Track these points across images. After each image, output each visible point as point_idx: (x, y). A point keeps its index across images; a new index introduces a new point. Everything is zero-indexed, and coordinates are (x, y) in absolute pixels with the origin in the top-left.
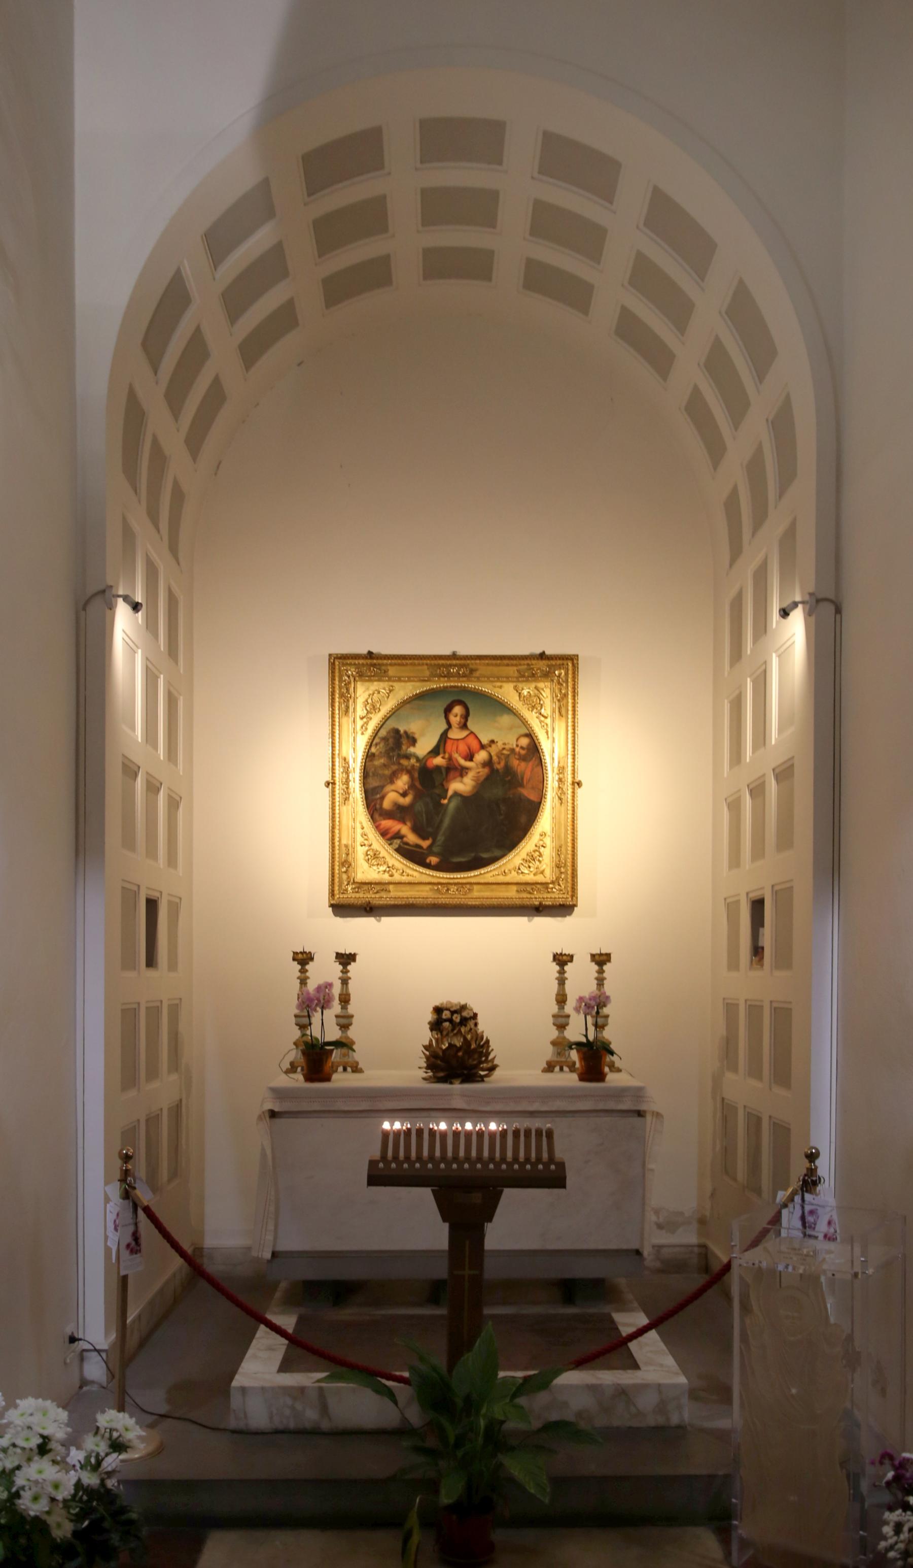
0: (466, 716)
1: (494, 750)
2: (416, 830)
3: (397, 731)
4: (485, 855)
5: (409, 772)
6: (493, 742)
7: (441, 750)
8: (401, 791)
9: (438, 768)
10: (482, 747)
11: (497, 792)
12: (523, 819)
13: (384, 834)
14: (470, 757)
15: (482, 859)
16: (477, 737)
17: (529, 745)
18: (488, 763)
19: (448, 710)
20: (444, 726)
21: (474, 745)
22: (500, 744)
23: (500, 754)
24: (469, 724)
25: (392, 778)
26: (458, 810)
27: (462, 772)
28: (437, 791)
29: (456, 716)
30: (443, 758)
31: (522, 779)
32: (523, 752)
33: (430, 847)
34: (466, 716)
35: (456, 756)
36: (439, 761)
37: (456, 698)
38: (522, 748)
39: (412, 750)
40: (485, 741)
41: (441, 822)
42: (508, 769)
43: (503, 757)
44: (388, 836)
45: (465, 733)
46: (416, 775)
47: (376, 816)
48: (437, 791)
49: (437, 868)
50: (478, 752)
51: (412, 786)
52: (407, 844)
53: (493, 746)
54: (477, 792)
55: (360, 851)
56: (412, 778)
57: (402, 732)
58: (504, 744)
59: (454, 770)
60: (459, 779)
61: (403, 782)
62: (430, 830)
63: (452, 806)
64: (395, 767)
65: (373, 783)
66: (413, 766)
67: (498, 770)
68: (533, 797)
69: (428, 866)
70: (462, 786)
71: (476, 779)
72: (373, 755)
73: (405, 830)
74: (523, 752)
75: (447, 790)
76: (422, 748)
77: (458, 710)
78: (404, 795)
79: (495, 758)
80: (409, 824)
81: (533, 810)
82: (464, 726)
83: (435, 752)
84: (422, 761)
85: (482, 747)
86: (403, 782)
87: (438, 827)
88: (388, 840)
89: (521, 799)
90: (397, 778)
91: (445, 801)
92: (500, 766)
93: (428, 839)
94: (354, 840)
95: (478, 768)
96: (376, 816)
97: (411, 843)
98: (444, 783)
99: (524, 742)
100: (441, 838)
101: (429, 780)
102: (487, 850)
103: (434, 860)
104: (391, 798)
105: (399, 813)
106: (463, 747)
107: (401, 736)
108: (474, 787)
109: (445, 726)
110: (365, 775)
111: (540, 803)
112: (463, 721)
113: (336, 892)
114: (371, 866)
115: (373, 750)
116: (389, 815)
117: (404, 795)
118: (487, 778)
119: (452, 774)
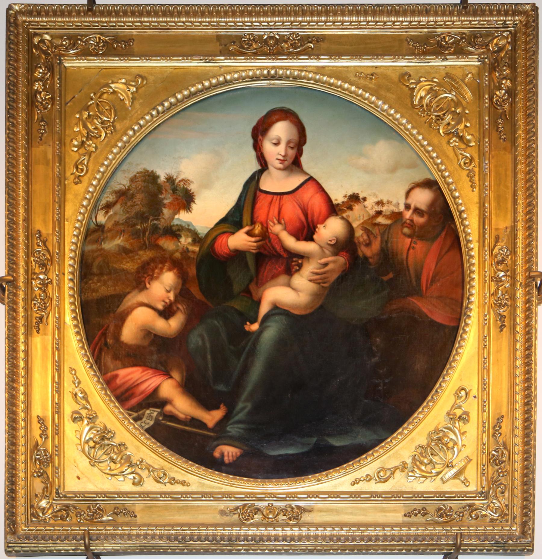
0: (299, 142)
1: (357, 217)
2: (189, 388)
3: (151, 177)
4: (336, 442)
5: (177, 264)
6: (355, 198)
7: (246, 218)
8: (160, 306)
9: (239, 255)
10: (333, 209)
11: (363, 307)
12: (420, 364)
13: (123, 396)
14: (306, 232)
15: (332, 448)
16: (321, 189)
17: (432, 204)
18: (346, 245)
19: (260, 131)
20: (254, 166)
21: (317, 204)
22: (370, 202)
23: (370, 224)
24: (304, 159)
25: (141, 279)
26: (281, 343)
27: (291, 263)
28: (237, 304)
29: (277, 144)
30: (249, 233)
31: (418, 278)
32: (420, 220)
33: (222, 423)
34: (299, 142)
35: (276, 228)
36: (240, 240)
37: (90, 171)
38: (417, 211)
39: (183, 217)
40: (338, 196)
41: (245, 370)
42: (388, 257)
43: (376, 231)
44: (134, 401)
45: (296, 181)
46: (192, 271)
47: (108, 359)
48: (237, 304)
49: (236, 469)
50: (323, 221)
51: (183, 293)
52: (172, 418)
53: (357, 207)
54: (321, 307)
55: (74, 434)
56: (183, 276)
57: (162, 178)
58: (380, 203)
59: (277, 261)
60: (283, 279)
61: (164, 285)
62: (221, 387)
63: (270, 334)
64: (146, 255)
65: (103, 289)
66: (185, 252)
67: (366, 258)
68: (439, 315)
69: (216, 465)
70: (289, 293)
71: (318, 279)
72: (100, 228)
73: (168, 388)
74: (420, 220)
75: (258, 303)
76: (207, 211)
77: (281, 130)
78: (166, 313)
79: (359, 233)
80: (176, 375)
81: (442, 344)
82: (294, 164)
83: (233, 221)
84: (208, 243)
85: (333, 209)
86: (164, 285)
87: (239, 385)
88: (132, 409)
89: (415, 321)
90: (152, 278)
91: (255, 327)
92: (370, 251)
93: (217, 408)
94: (58, 409)
95: (324, 255)
96: (108, 359)
97: (182, 416)
98: (252, 287)
99: (422, 198)
100: (244, 406)
101: (220, 279)
102: (342, 433)
103: (229, 452)
104: (140, 319)
105: (156, 351)
106: (291, 210)
107: (160, 189)
108: (316, 296)
109: (255, 166)
110: (86, 269)
111: (456, 329)
112: (292, 153)
113: (21, 519)
114: (94, 462)
115: (101, 218)
116: (134, 356)
117: (166, 313)
118: (344, 277)
119: (268, 268)
